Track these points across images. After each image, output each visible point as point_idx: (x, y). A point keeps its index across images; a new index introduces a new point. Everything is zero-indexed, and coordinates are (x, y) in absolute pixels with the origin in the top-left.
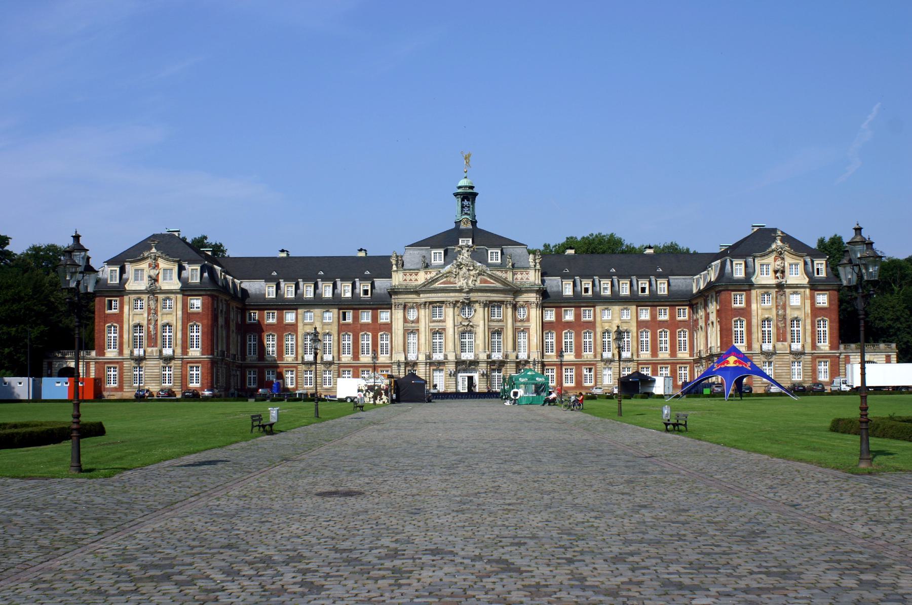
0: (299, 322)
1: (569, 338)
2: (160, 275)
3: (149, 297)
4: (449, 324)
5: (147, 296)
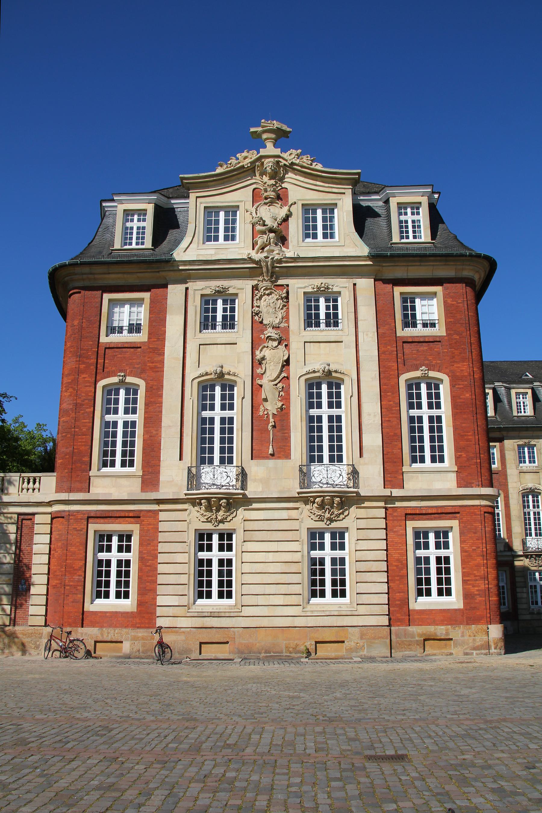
0: (508, 466)
2: (292, 221)
3: (255, 288)
5: (248, 284)
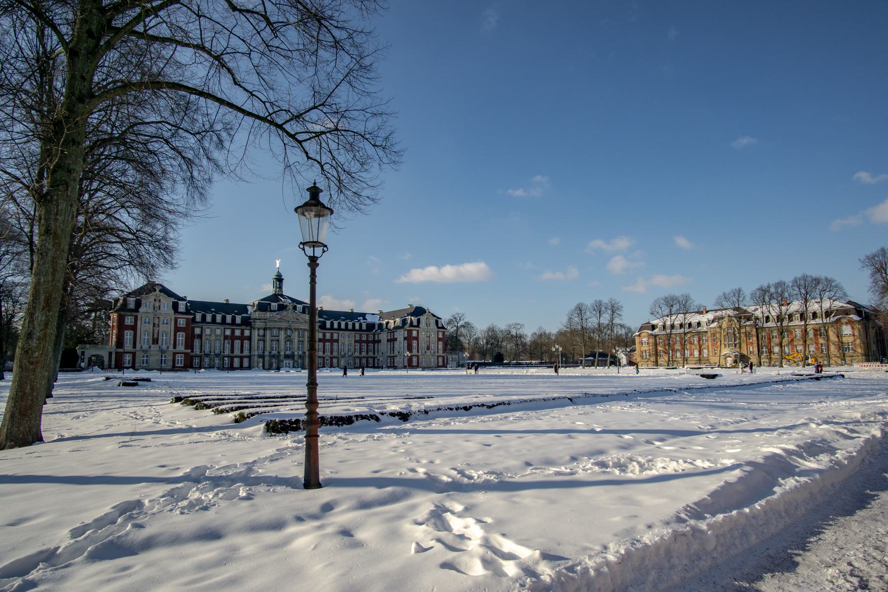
1: (328, 344)
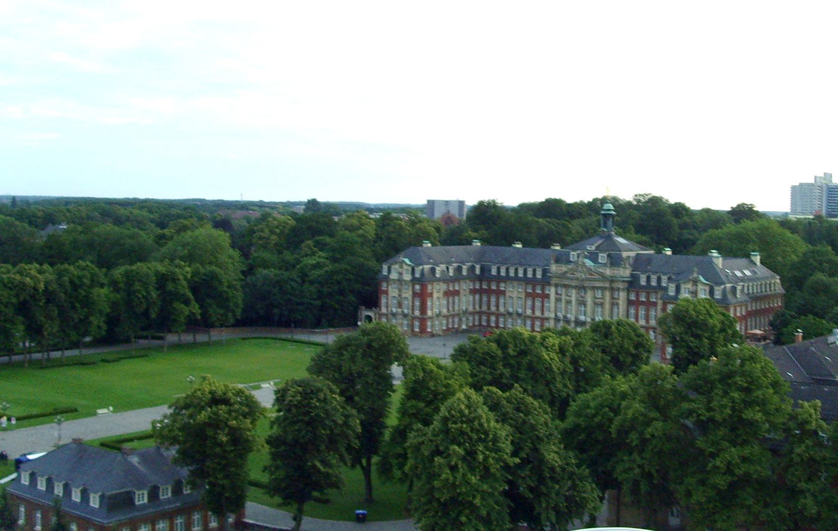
4: (573, 299)
